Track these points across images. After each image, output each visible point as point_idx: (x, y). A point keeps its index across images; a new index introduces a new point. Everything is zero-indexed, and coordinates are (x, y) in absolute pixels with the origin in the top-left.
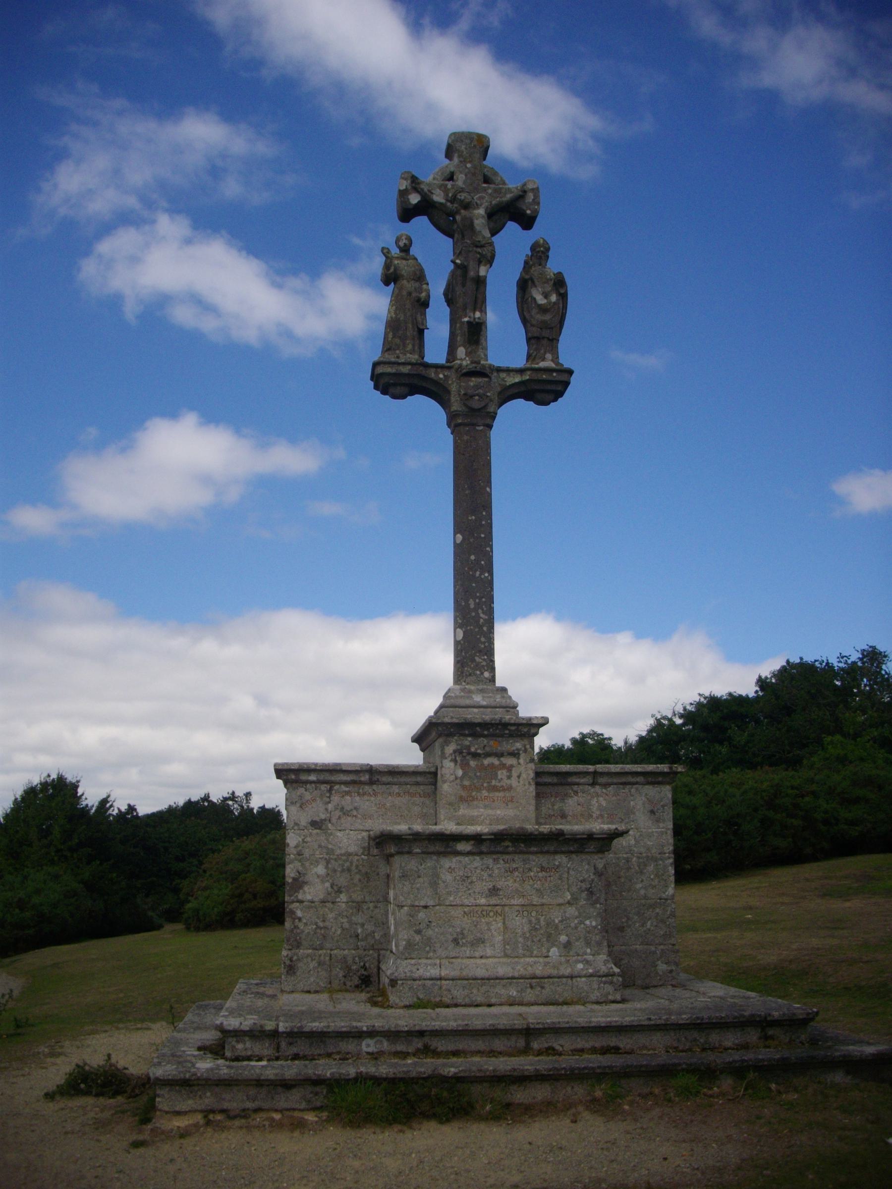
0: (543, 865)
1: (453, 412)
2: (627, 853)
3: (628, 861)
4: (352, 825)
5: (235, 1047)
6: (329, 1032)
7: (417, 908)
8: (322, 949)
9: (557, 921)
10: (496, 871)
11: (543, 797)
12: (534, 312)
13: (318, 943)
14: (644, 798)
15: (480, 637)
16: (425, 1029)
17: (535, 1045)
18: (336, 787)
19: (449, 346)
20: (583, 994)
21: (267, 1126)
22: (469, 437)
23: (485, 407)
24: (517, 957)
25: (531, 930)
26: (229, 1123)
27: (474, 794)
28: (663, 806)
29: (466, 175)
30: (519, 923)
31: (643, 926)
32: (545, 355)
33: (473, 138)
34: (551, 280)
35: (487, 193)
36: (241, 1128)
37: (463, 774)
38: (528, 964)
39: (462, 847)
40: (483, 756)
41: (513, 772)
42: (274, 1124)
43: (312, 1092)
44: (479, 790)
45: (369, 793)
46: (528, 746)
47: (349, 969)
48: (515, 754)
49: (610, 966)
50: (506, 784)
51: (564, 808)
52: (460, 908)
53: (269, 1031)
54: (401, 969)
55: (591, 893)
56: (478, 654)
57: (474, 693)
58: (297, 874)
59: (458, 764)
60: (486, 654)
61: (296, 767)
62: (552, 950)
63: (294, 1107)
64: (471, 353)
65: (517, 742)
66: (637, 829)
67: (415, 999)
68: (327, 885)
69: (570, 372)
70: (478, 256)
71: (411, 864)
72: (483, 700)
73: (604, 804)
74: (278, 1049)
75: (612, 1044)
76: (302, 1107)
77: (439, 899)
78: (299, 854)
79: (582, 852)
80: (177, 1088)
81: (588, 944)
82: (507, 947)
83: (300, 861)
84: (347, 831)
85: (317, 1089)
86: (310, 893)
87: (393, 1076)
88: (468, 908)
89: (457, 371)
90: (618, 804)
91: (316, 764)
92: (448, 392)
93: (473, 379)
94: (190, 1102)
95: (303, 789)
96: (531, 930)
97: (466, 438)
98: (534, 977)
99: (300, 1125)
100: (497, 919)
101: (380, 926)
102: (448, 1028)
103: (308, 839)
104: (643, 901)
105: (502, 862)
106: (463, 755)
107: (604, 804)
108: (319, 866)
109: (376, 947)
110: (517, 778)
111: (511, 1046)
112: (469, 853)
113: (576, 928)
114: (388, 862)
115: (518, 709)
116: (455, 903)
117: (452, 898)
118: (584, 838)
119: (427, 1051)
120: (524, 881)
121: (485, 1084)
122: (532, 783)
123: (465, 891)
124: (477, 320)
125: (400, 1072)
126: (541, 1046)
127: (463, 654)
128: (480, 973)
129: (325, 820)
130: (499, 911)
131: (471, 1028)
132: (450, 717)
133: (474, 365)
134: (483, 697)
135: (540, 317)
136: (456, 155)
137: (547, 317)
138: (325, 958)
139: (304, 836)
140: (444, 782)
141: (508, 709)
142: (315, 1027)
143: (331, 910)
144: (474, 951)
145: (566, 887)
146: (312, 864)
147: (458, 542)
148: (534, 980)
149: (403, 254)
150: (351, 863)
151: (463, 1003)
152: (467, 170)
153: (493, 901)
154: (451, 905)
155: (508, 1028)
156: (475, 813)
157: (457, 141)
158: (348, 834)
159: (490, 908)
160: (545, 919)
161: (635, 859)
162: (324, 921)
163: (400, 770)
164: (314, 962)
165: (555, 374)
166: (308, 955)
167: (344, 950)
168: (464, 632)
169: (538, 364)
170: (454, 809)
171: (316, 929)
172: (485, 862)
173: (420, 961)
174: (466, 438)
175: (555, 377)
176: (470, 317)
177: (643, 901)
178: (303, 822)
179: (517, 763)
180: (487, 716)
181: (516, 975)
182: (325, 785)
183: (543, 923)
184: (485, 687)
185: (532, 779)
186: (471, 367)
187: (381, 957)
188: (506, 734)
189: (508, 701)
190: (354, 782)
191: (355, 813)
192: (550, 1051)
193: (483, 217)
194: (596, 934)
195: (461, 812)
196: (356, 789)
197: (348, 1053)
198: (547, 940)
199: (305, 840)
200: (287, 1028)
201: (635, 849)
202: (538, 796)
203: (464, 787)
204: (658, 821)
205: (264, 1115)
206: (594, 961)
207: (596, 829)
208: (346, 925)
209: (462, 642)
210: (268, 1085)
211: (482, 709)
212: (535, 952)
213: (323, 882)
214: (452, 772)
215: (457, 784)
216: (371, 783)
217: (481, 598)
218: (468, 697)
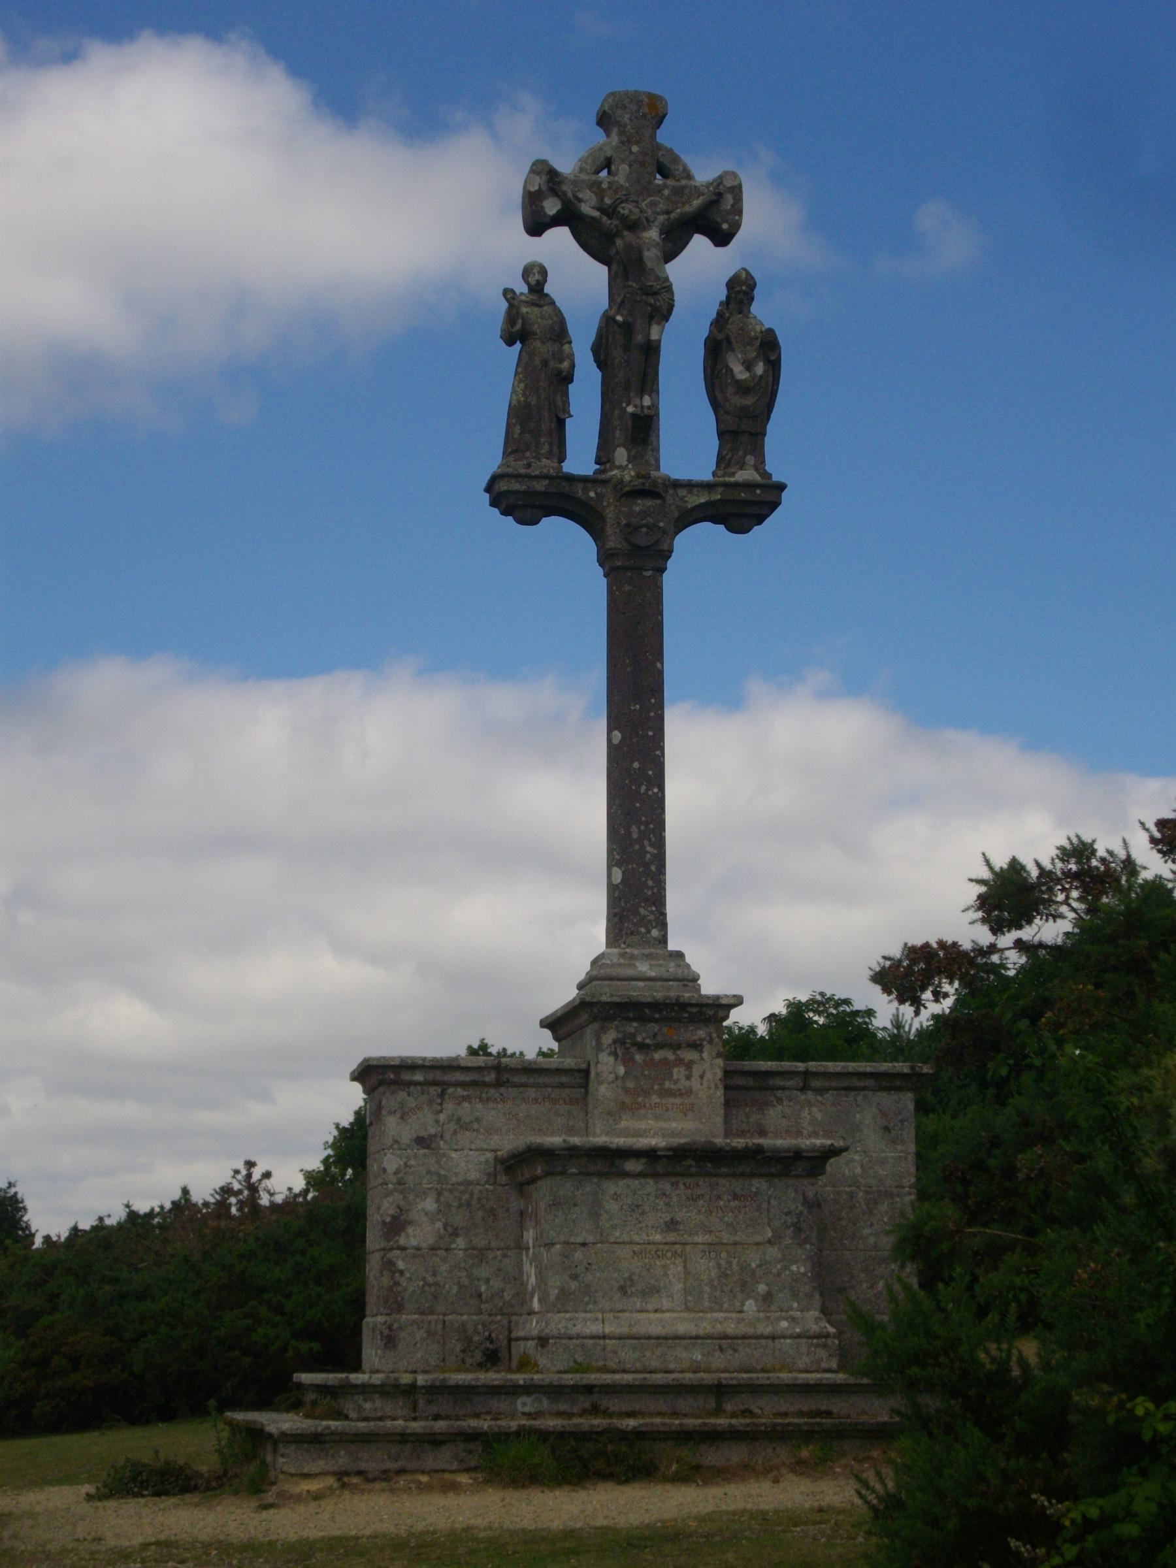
0: (737, 1191)
1: (609, 550)
2: (850, 1186)
3: (852, 1197)
4: (472, 1142)
5: (362, 1406)
6: (477, 1386)
7: (573, 1246)
8: (431, 1313)
9: (754, 1265)
10: (675, 1199)
11: (734, 1106)
12: (730, 390)
13: (427, 1305)
14: (874, 1109)
15: (647, 880)
16: (594, 1382)
17: (729, 1407)
18: (451, 1090)
19: (601, 435)
20: (788, 1360)
21: (413, 1489)
22: (631, 588)
23: (656, 543)
24: (702, 1312)
25: (721, 1276)
26: (369, 1486)
27: (640, 1099)
28: (902, 1121)
29: (630, 166)
30: (704, 1267)
31: (872, 1287)
32: (745, 458)
33: (642, 101)
34: (756, 338)
35: (663, 195)
36: (383, 1490)
37: (625, 1073)
38: (717, 1320)
39: (631, 1166)
40: (653, 1048)
41: (694, 1070)
42: (422, 1487)
43: (465, 1451)
44: (646, 1093)
45: (496, 1099)
46: (714, 1035)
47: (469, 1340)
48: (696, 1046)
49: (823, 1325)
50: (685, 1086)
51: (763, 1122)
52: (627, 1246)
53: (405, 1385)
54: (552, 1325)
55: (798, 1229)
56: (643, 904)
57: (638, 960)
58: (398, 1211)
59: (619, 1059)
60: (654, 904)
61: (397, 1063)
62: (747, 1303)
63: (442, 1467)
64: (635, 457)
65: (699, 1028)
66: (865, 1152)
67: (572, 1364)
68: (439, 1225)
69: (781, 487)
70: (649, 309)
71: (565, 1188)
72: (650, 969)
73: (819, 1116)
74: (415, 1409)
75: (824, 1408)
76: (453, 1468)
77: (601, 1235)
78: (400, 1183)
79: (787, 1175)
80: (305, 1446)
81: (795, 1295)
82: (689, 1298)
83: (401, 1192)
84: (465, 1151)
85: (471, 1446)
86: (414, 1236)
87: (562, 1429)
88: (639, 1246)
89: (615, 487)
90: (838, 1116)
91: (424, 1059)
92: (602, 518)
93: (639, 501)
94: (321, 1463)
95: (405, 1093)
96: (721, 1276)
97: (627, 588)
98: (725, 1337)
99: (454, 1487)
100: (677, 1262)
101: (510, 1283)
102: (622, 1383)
103: (413, 1162)
104: (873, 1254)
105: (682, 1187)
106: (625, 1047)
107: (819, 1116)
108: (427, 1200)
109: (506, 1311)
110: (699, 1079)
111: (698, 1408)
112: (640, 1175)
113: (779, 1274)
114: (521, 1193)
115: (699, 982)
116: (621, 1240)
117: (617, 1234)
118: (789, 1157)
119: (595, 1410)
120: (711, 1212)
121: (669, 1443)
122: (720, 1086)
123: (635, 1225)
124: (646, 411)
125: (569, 1425)
126: (735, 1408)
127: (623, 904)
128: (656, 1330)
129: (435, 1136)
130: (679, 1251)
131: (650, 1383)
132: (607, 993)
133: (640, 480)
134: (651, 965)
135: (738, 401)
136: (615, 130)
137: (749, 401)
138: (436, 1326)
139: (407, 1157)
140: (601, 1083)
141: (686, 983)
142: (461, 1379)
143: (444, 1260)
144: (646, 1303)
145: (766, 1220)
146: (417, 1196)
147: (616, 741)
148: (724, 1341)
149: (533, 297)
150: (472, 1195)
151: (633, 1369)
152: (632, 158)
153: (672, 1237)
154: (616, 1243)
155: (694, 1383)
156: (643, 1125)
157: (617, 107)
158: (467, 1155)
159: (666, 1247)
160: (738, 1261)
161: (861, 1194)
162: (434, 1275)
163: (538, 1067)
164: (422, 1331)
165: (758, 491)
166: (414, 1322)
167: (462, 1315)
168: (623, 872)
169: (733, 474)
170: (614, 1120)
171: (424, 1286)
172: (661, 1186)
173: (577, 1315)
174: (627, 588)
175: (759, 495)
176: (635, 406)
177: (873, 1254)
178: (406, 1140)
179: (699, 1058)
180: (659, 993)
181: (701, 1332)
182: (436, 1088)
183: (735, 1267)
184: (653, 950)
185: (720, 1080)
186: (636, 483)
187: (513, 1325)
188: (686, 1018)
189: (686, 971)
190: (474, 1084)
191: (476, 1126)
192: (746, 1412)
193: (658, 244)
194: (806, 1284)
195: (624, 1124)
196: (478, 1093)
197: (500, 1414)
198: (741, 1290)
199: (408, 1164)
200: (427, 1381)
201: (861, 1180)
202: (728, 1104)
203: (627, 1091)
204: (894, 1141)
205: (409, 1477)
206: (802, 1318)
207: (806, 1145)
208: (465, 1281)
209: (621, 887)
210: (413, 1442)
211: (648, 983)
212: (726, 1306)
213: (433, 1221)
214: (611, 1069)
215: (617, 1086)
216: (498, 1084)
217: (647, 824)
218: (630, 965)
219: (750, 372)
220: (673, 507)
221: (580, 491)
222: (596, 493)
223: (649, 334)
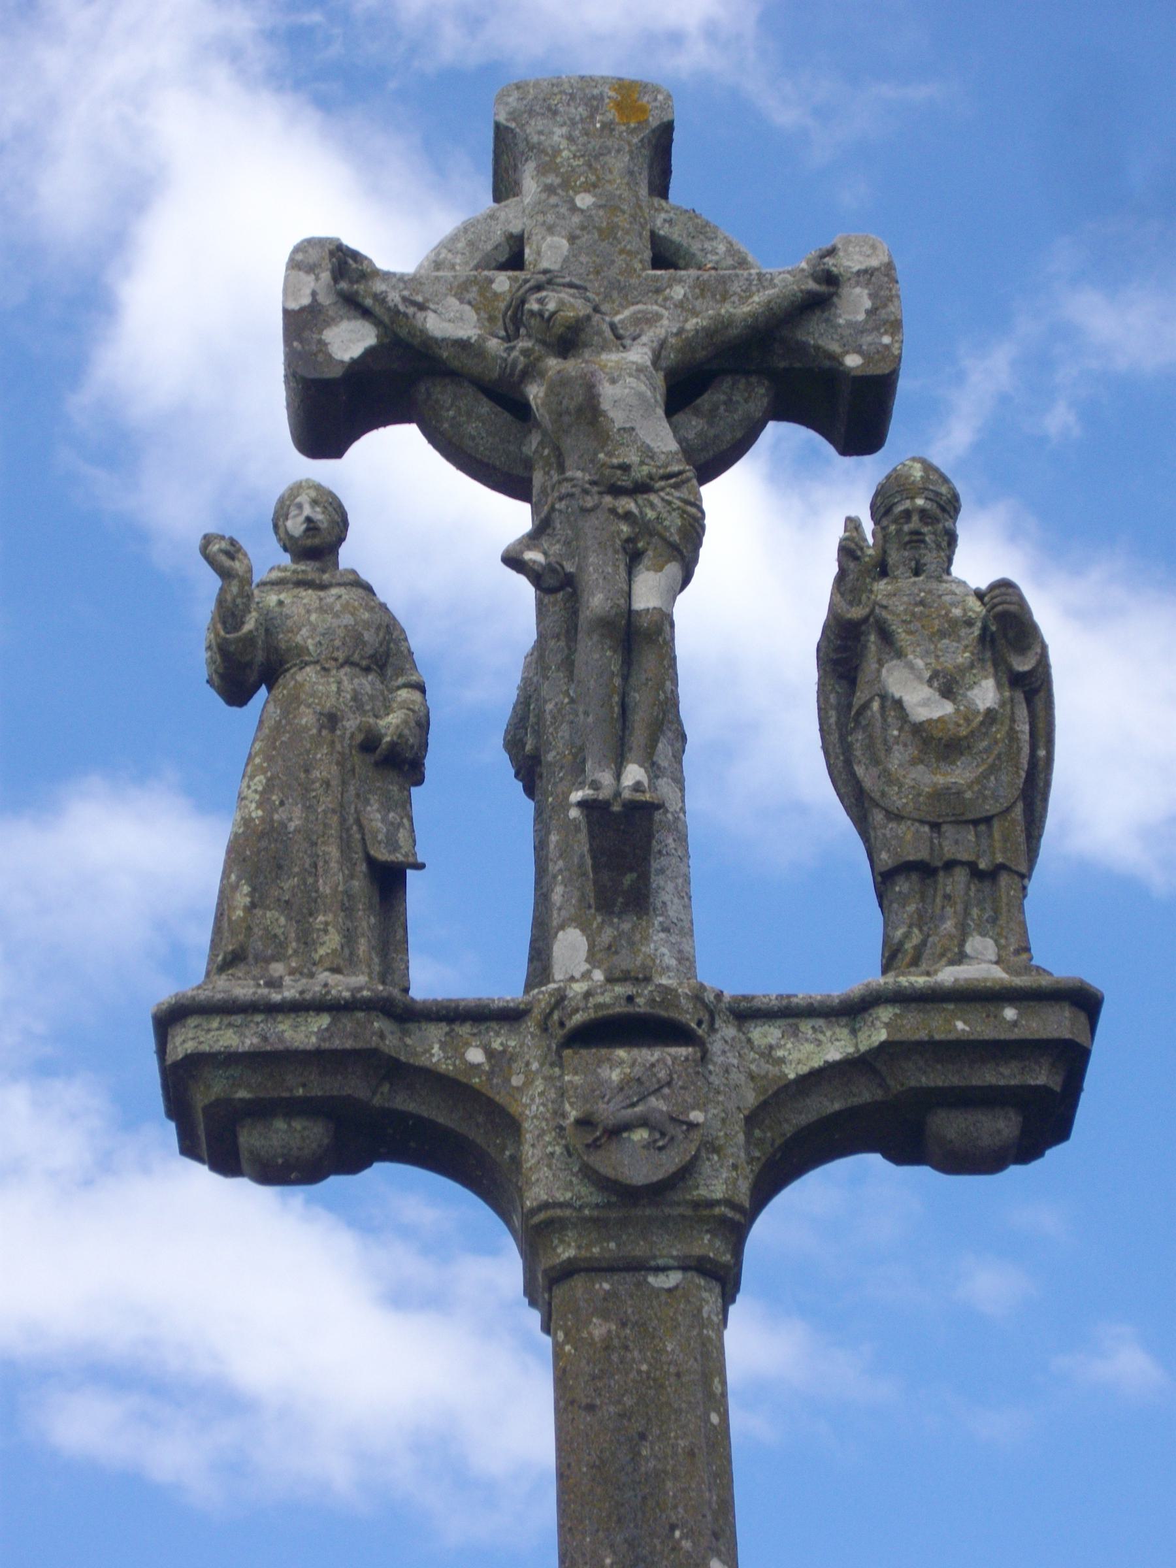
1: (534, 1211)
29: (572, 239)
70: (625, 528)
97: (599, 1329)
165: (1010, 1013)
174: (599, 1329)
175: (1015, 1024)
186: (606, 998)
219: (954, 701)
220: (737, 1077)
221: (436, 1049)
222: (490, 1053)
223: (629, 595)
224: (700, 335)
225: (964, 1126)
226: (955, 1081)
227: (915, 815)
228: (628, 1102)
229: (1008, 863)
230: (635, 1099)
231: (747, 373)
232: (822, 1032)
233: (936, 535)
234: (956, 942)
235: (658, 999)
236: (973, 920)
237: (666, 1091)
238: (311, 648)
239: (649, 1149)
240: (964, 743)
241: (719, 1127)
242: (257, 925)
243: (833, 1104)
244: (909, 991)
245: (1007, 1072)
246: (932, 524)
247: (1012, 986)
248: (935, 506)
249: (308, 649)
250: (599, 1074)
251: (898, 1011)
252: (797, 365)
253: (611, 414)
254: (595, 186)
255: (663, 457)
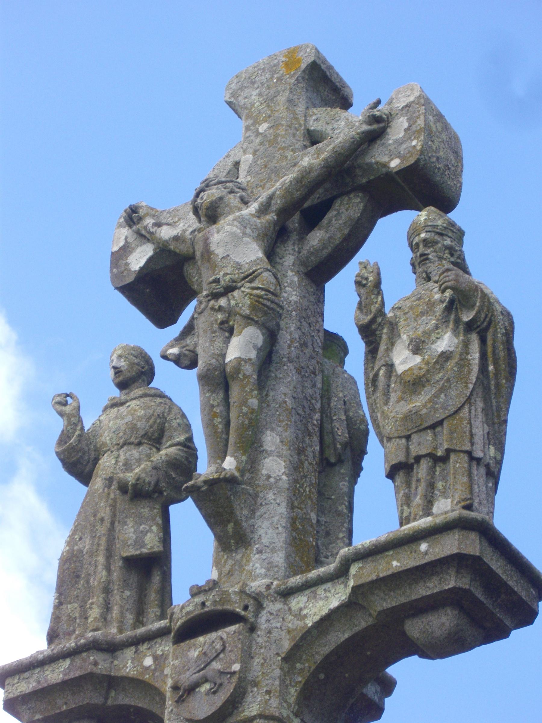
165: (424, 547)
175: (426, 553)
224: (293, 183)
225: (422, 627)
226: (403, 600)
227: (396, 435)
228: (198, 669)
229: (452, 447)
230: (203, 666)
231: (348, 193)
232: (329, 591)
233: (437, 252)
234: (421, 508)
235: (218, 600)
236: (439, 490)
237: (222, 656)
238: (108, 442)
239: (209, 695)
240: (424, 379)
241: (259, 670)
242: (64, 614)
243: (344, 635)
244: (362, 551)
245: (431, 585)
246: (432, 246)
247: (419, 529)
248: (433, 234)
249: (107, 443)
250: (188, 656)
251: (361, 565)
252: (372, 178)
253: (216, 252)
254: (270, 117)
255: (247, 266)
